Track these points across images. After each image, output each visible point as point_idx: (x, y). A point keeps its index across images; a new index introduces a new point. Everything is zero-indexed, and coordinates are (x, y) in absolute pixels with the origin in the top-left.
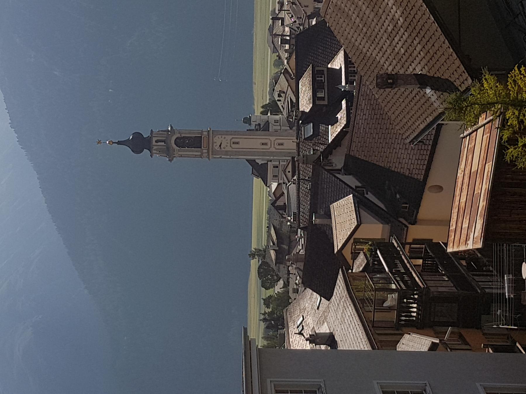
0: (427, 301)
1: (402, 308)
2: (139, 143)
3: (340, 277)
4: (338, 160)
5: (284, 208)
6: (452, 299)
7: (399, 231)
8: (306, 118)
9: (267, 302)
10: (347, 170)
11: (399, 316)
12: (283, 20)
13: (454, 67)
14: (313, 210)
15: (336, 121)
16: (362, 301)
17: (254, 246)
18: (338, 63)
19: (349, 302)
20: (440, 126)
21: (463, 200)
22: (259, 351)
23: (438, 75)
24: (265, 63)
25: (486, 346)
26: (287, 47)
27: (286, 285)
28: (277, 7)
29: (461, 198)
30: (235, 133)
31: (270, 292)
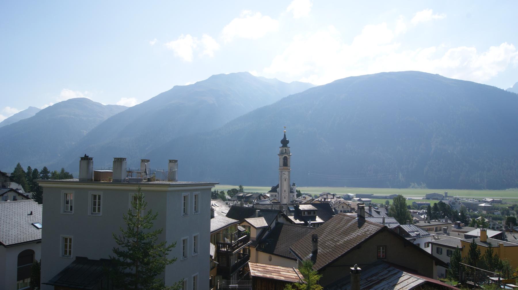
0: (227, 255)
1: (224, 245)
2: (285, 142)
3: (236, 221)
4: (281, 220)
5: (260, 199)
6: (229, 265)
7: (254, 244)
8: (297, 208)
9: (222, 192)
10: (277, 224)
11: (221, 244)
12: (333, 198)
13: (321, 264)
14: (262, 210)
15: (296, 219)
16: (227, 229)
17: (245, 187)
18: (318, 220)
19: (226, 224)
20: (296, 260)
21: (269, 268)
22: (210, 189)
23: (318, 258)
24: (315, 191)
25: (212, 277)
26: (323, 200)
27: (229, 200)
28: (338, 196)
29: (270, 268)
30: (289, 180)
31: (226, 194)
